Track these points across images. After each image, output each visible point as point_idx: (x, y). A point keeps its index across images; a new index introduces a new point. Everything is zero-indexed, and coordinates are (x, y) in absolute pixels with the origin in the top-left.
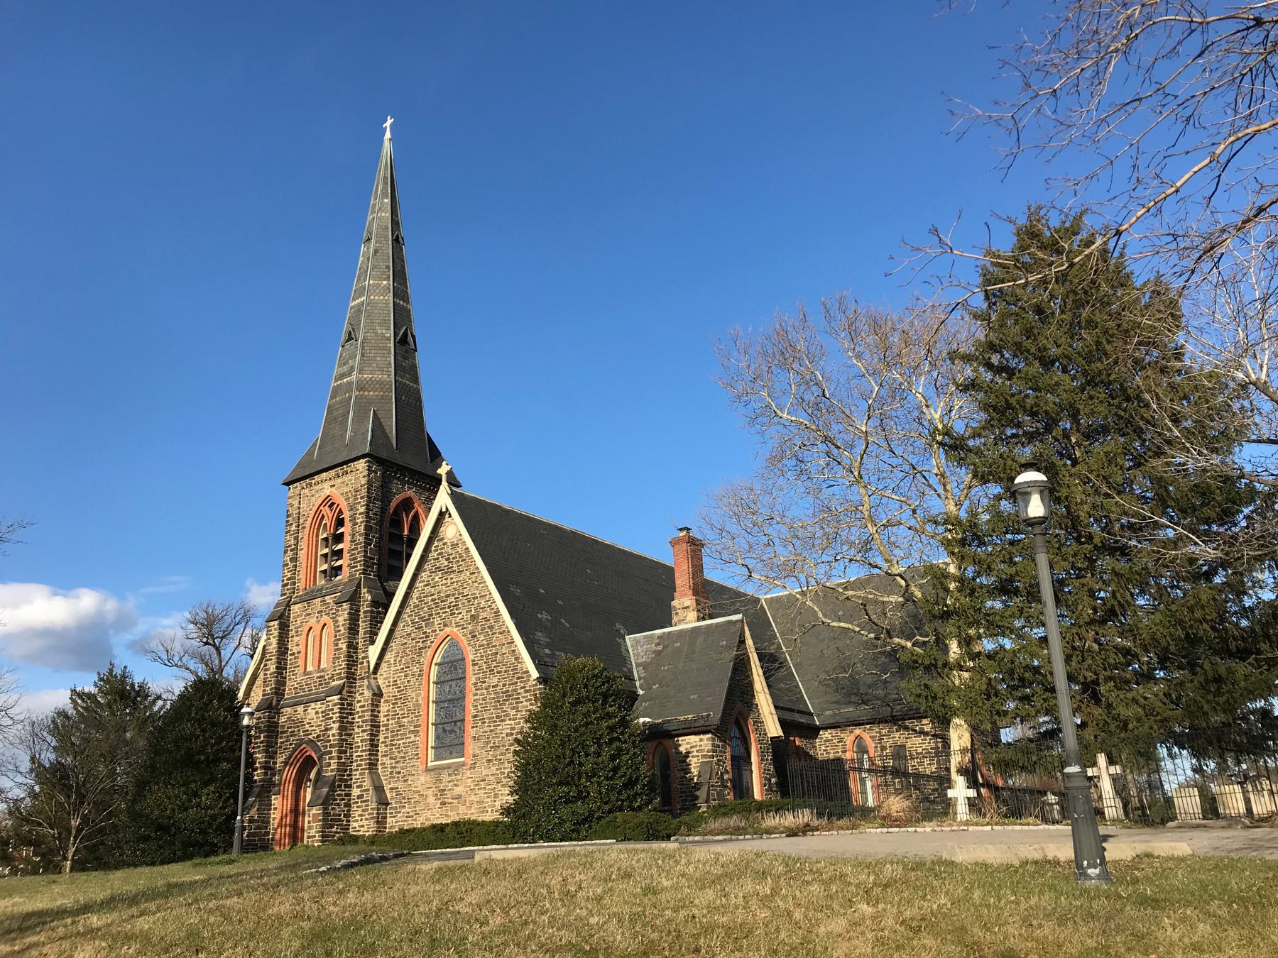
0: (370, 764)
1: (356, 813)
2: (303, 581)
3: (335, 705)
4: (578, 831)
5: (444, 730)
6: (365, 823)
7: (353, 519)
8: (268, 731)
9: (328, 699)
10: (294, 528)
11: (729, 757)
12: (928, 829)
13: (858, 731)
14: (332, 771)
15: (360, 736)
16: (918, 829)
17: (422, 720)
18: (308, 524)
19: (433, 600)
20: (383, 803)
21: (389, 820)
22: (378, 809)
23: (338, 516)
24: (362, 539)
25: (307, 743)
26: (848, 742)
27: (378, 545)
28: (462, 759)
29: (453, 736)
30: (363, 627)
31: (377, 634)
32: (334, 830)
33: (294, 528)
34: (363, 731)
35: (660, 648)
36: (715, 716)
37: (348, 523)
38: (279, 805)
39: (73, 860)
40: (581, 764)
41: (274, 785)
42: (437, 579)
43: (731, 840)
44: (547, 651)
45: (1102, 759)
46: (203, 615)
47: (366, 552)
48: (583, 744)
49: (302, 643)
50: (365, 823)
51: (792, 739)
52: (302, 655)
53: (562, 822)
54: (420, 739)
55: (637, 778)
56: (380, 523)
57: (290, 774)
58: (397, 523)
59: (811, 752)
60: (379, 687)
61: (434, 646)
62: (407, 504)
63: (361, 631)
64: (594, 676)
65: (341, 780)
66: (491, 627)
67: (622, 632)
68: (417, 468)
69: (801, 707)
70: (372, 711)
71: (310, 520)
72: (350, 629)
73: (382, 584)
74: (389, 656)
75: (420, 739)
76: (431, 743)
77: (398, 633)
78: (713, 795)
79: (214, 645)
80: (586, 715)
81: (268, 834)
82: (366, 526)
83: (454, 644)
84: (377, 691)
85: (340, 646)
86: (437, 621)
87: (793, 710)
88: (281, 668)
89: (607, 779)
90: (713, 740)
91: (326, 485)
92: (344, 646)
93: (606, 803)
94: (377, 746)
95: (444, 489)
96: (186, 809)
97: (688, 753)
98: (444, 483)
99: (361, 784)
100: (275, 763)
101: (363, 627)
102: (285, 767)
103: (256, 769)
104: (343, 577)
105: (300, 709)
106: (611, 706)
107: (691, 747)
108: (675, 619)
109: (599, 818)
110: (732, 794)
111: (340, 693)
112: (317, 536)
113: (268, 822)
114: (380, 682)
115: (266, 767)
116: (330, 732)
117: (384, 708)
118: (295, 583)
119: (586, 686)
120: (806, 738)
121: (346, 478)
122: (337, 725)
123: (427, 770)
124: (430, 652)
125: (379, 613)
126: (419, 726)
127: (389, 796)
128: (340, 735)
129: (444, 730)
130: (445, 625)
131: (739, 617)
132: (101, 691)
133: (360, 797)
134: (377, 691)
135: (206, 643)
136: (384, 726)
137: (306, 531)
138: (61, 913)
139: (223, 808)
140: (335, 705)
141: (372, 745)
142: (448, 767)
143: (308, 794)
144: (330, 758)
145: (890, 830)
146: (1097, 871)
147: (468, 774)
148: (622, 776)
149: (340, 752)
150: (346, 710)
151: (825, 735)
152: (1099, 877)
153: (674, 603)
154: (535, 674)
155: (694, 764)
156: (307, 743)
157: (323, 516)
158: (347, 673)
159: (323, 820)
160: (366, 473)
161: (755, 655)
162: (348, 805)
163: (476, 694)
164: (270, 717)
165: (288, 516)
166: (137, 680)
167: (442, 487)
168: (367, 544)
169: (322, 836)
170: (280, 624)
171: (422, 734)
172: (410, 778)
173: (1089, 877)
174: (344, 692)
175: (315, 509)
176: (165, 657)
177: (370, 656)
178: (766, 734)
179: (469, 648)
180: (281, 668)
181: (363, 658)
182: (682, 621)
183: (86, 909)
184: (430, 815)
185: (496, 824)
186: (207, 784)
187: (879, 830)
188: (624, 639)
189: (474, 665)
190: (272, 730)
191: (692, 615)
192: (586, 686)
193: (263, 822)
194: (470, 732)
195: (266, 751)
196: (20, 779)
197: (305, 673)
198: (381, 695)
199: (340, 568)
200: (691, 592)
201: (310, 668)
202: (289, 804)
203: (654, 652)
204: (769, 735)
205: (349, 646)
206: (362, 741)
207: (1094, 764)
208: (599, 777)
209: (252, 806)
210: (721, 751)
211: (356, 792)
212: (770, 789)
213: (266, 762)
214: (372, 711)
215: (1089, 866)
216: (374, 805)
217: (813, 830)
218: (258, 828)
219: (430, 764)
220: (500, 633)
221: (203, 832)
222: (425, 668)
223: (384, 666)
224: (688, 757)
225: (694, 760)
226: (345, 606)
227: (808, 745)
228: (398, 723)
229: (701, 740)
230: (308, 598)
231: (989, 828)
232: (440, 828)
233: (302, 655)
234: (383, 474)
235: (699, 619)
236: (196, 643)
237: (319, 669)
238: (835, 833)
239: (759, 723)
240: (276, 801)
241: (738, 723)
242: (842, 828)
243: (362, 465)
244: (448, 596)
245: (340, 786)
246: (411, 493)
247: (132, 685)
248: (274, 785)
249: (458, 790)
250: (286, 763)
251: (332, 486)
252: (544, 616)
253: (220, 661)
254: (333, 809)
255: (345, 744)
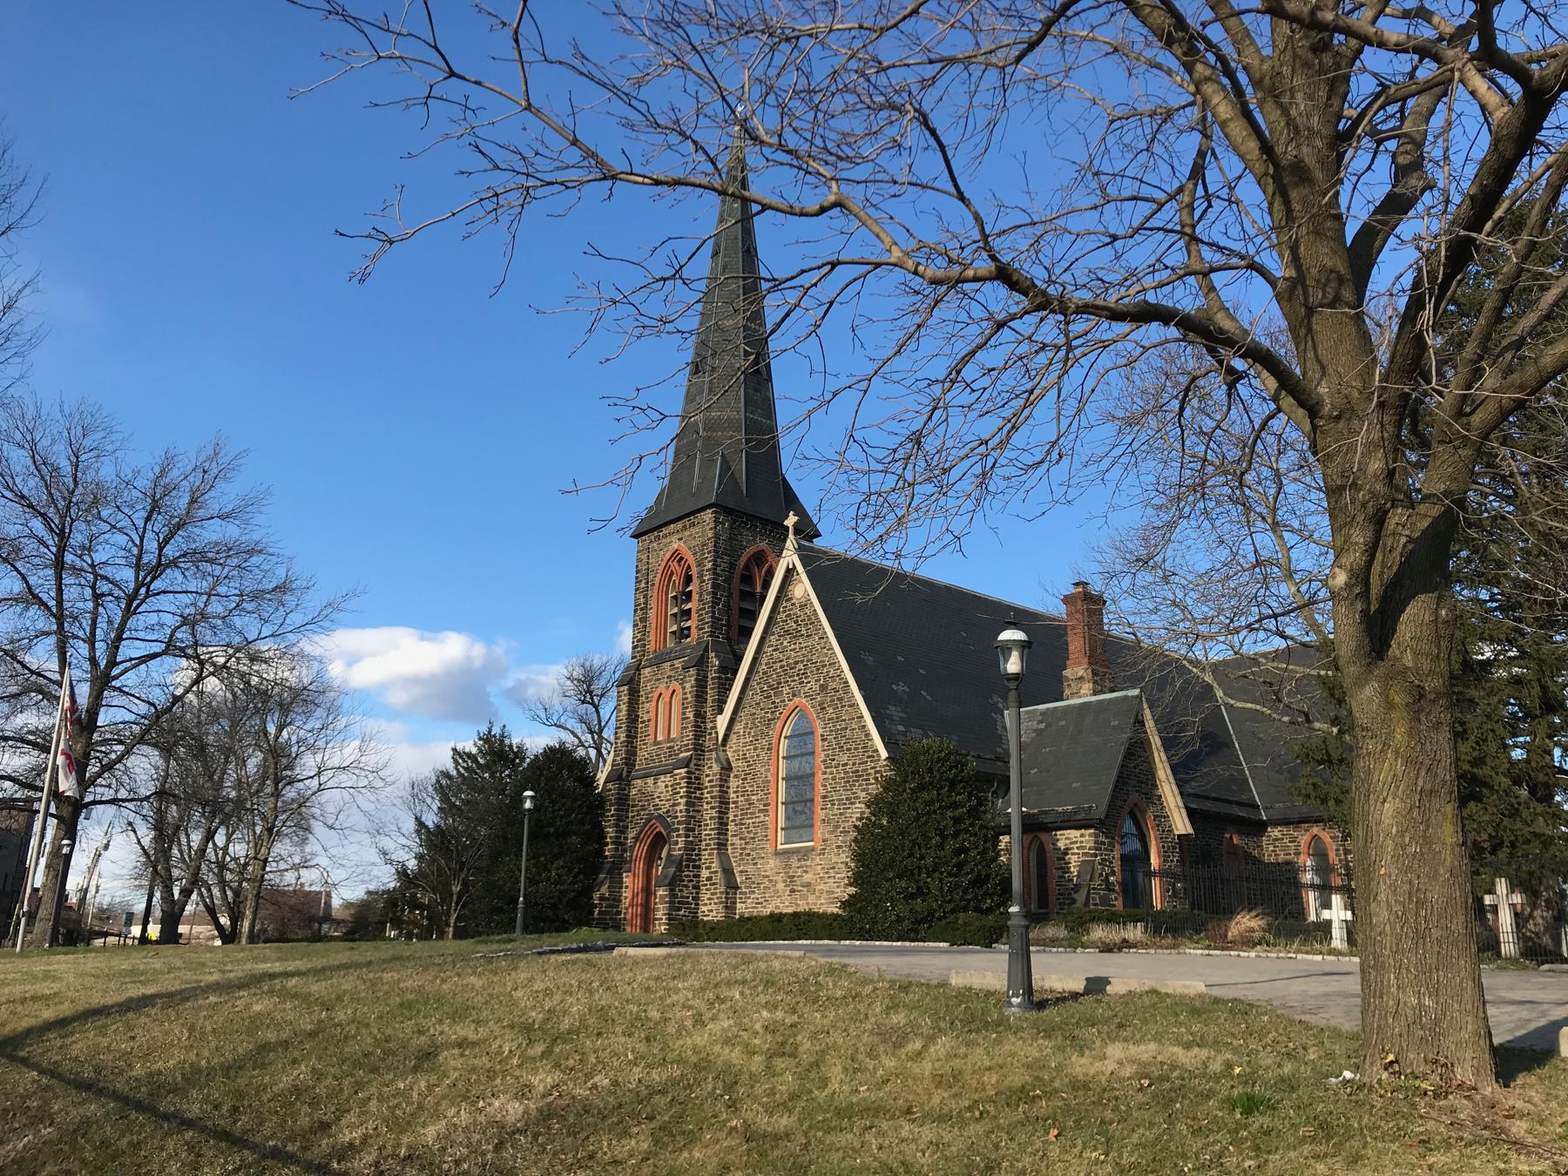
0: (719, 844)
1: (705, 896)
2: (653, 643)
3: (682, 779)
4: (917, 931)
5: (795, 811)
6: (713, 907)
7: (701, 576)
8: (619, 804)
9: (676, 772)
10: (643, 585)
11: (1117, 856)
12: (1253, 954)
13: (1315, 830)
14: (680, 849)
15: (709, 813)
16: (1242, 954)
17: (772, 797)
18: (657, 581)
19: (781, 667)
20: (732, 886)
21: (738, 906)
22: (727, 893)
23: (687, 572)
24: (708, 598)
25: (656, 818)
26: (1302, 843)
27: (727, 606)
28: (811, 844)
29: (803, 817)
30: (711, 695)
31: (725, 702)
32: (682, 913)
33: (643, 585)
34: (712, 808)
35: (1042, 726)
36: (1099, 809)
37: (695, 580)
38: (631, 883)
39: (455, 926)
40: (922, 857)
41: (625, 862)
42: (785, 644)
43: (980, 952)
44: (901, 728)
45: (1501, 886)
46: (581, 670)
47: (713, 612)
48: (924, 835)
49: (653, 710)
50: (713, 907)
51: (1228, 836)
52: (652, 723)
53: (899, 920)
54: (769, 819)
55: (988, 877)
56: (729, 580)
57: (641, 851)
58: (748, 579)
59: (1256, 853)
60: (728, 761)
61: (783, 717)
62: (759, 558)
63: (710, 699)
64: (939, 760)
65: (688, 860)
66: (840, 699)
67: (1000, 706)
68: (770, 517)
69: (1244, 798)
70: (721, 786)
71: (659, 576)
72: (697, 696)
73: (731, 647)
74: (738, 727)
75: (769, 819)
76: (781, 823)
77: (747, 700)
78: (1094, 899)
79: (593, 704)
80: (929, 803)
81: (620, 913)
82: (713, 584)
83: (803, 714)
84: (725, 765)
85: (688, 715)
86: (786, 690)
87: (1230, 802)
88: (631, 736)
89: (950, 875)
90: (1096, 836)
91: (674, 538)
92: (691, 715)
93: (949, 902)
94: (727, 824)
95: (791, 542)
96: (537, 883)
97: (1068, 849)
98: (791, 536)
99: (710, 866)
100: (626, 838)
101: (711, 695)
102: (635, 843)
103: (607, 844)
104: (692, 640)
105: (650, 781)
106: (960, 794)
107: (1071, 843)
108: (1067, 692)
109: (939, 919)
110: (1121, 899)
111: (687, 766)
112: (667, 594)
113: (620, 901)
114: (730, 754)
115: (618, 842)
116: (678, 808)
117: (733, 783)
118: (644, 645)
119: (930, 770)
120: (1248, 835)
121: (693, 530)
122: (683, 801)
123: (777, 853)
124: (779, 724)
125: (727, 679)
126: (768, 805)
127: (738, 880)
128: (687, 811)
129: (795, 811)
130: (794, 695)
131: (1136, 692)
132: (481, 751)
133: (709, 879)
134: (725, 765)
135: (583, 702)
136: (734, 803)
137: (656, 588)
138: (273, 976)
139: (573, 883)
140: (682, 779)
141: (721, 824)
142: (797, 851)
143: (659, 870)
144: (678, 836)
145: (1212, 952)
146: (1019, 1000)
147: (818, 860)
148: (968, 873)
149: (687, 829)
150: (694, 784)
151: (1275, 832)
152: (1019, 1005)
153: (1067, 673)
154: (884, 754)
155: (1074, 861)
156: (656, 818)
157: (672, 573)
158: (695, 744)
159: (670, 902)
160: (712, 525)
161: (1157, 739)
162: (697, 887)
163: (825, 773)
164: (620, 789)
165: (637, 572)
166: (515, 741)
167: (788, 541)
168: (715, 603)
169: (669, 919)
170: (630, 690)
171: (772, 814)
172: (760, 861)
173: (1010, 1005)
174: (692, 765)
175: (663, 564)
176: (543, 716)
177: (719, 726)
178: (1171, 831)
179: (818, 722)
180: (631, 736)
181: (712, 728)
182: (1076, 694)
183: (287, 975)
184: (783, 904)
185: (835, 917)
186: (556, 857)
187: (1199, 952)
188: (1002, 715)
189: (823, 740)
190: (623, 801)
191: (1087, 687)
192: (930, 770)
193: (614, 900)
194: (820, 814)
195: (617, 825)
196: (404, 841)
197: (656, 743)
198: (730, 768)
199: (689, 628)
200: (1086, 660)
201: (660, 738)
202: (640, 883)
203: (1035, 731)
204: (1176, 833)
205: (696, 716)
206: (711, 819)
207: (1491, 891)
208: (942, 873)
209: (602, 883)
210: (1106, 849)
211: (705, 874)
212: (1175, 895)
213: (616, 837)
214: (721, 786)
215: (1013, 996)
216: (723, 889)
217: (1130, 947)
218: (611, 906)
219: (779, 847)
220: (850, 706)
221: (553, 907)
222: (774, 741)
223: (733, 737)
224: (1067, 854)
225: (1075, 858)
226: (692, 671)
227: (1251, 844)
228: (747, 800)
229: (1082, 836)
230: (658, 661)
231: (1319, 958)
232: (777, 918)
233: (652, 723)
234: (731, 527)
235: (1095, 693)
236: (573, 701)
237: (669, 740)
238: (1153, 951)
239: (1162, 818)
240: (627, 879)
241: (1132, 815)
242: (1162, 948)
243: (708, 516)
244: (796, 663)
245: (687, 866)
246: (763, 545)
247: (511, 746)
248: (625, 862)
249: (808, 877)
250: (636, 839)
251: (680, 539)
252: (901, 688)
253: (600, 721)
254: (681, 891)
255: (693, 821)
